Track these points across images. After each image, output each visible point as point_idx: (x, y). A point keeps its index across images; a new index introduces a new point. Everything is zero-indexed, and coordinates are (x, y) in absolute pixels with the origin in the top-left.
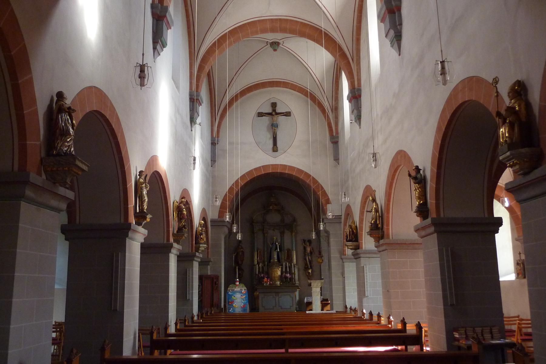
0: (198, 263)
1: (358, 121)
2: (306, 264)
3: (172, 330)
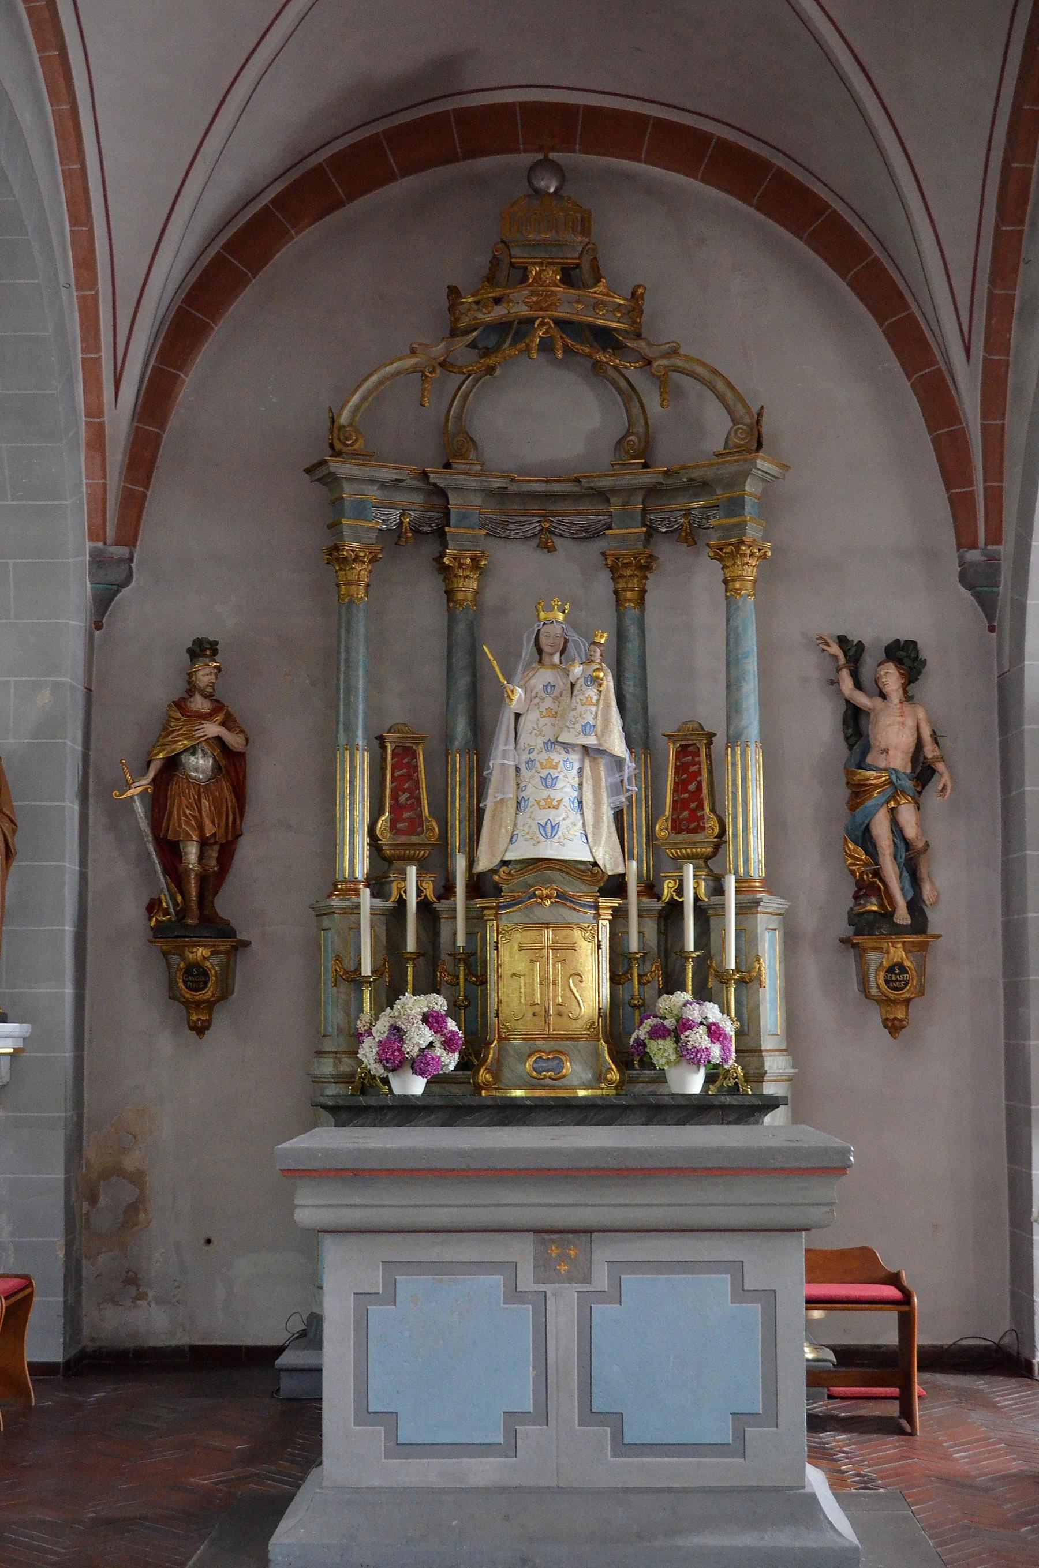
2: (870, 885)
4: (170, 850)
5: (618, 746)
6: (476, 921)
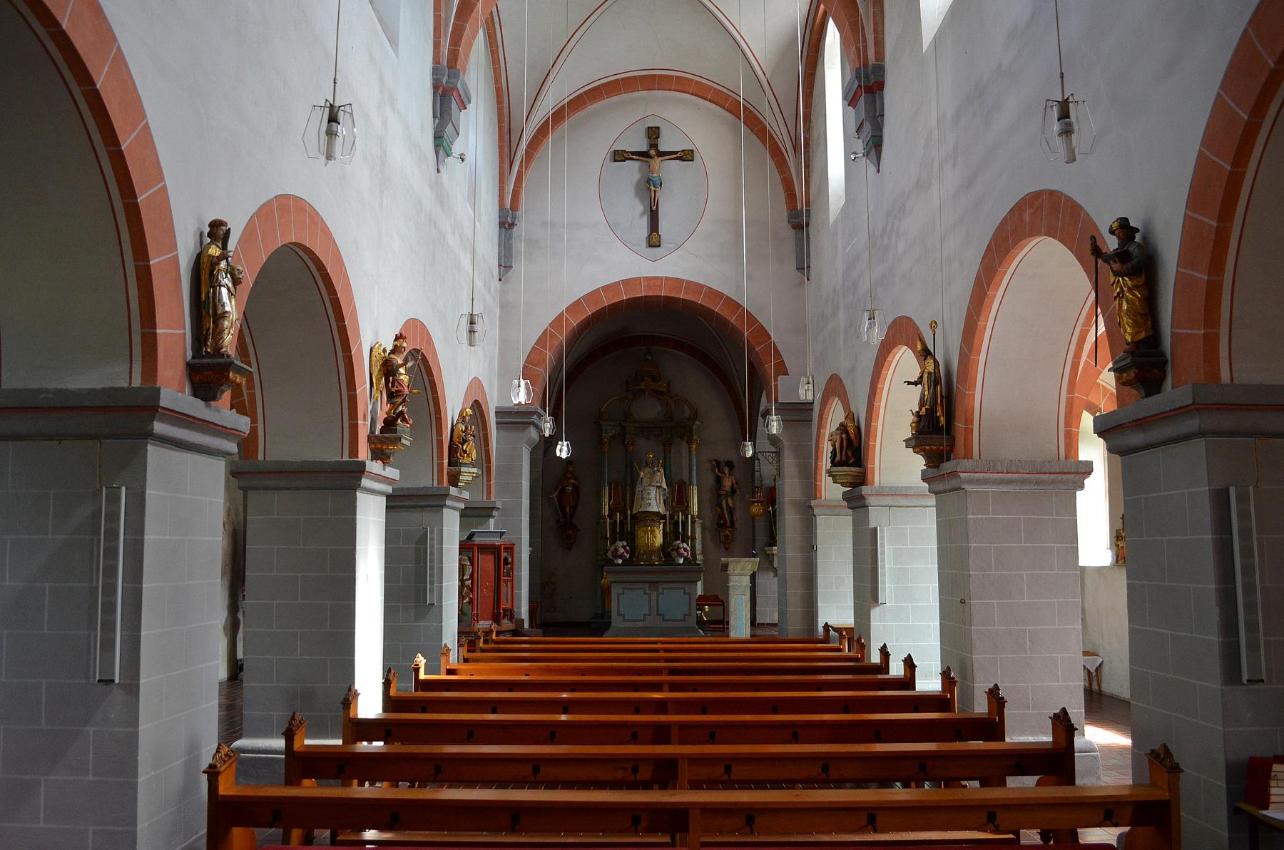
0: (457, 514)
1: (873, 152)
2: (721, 517)
3: (370, 705)
4: (563, 509)
5: (664, 486)
6: (633, 525)
